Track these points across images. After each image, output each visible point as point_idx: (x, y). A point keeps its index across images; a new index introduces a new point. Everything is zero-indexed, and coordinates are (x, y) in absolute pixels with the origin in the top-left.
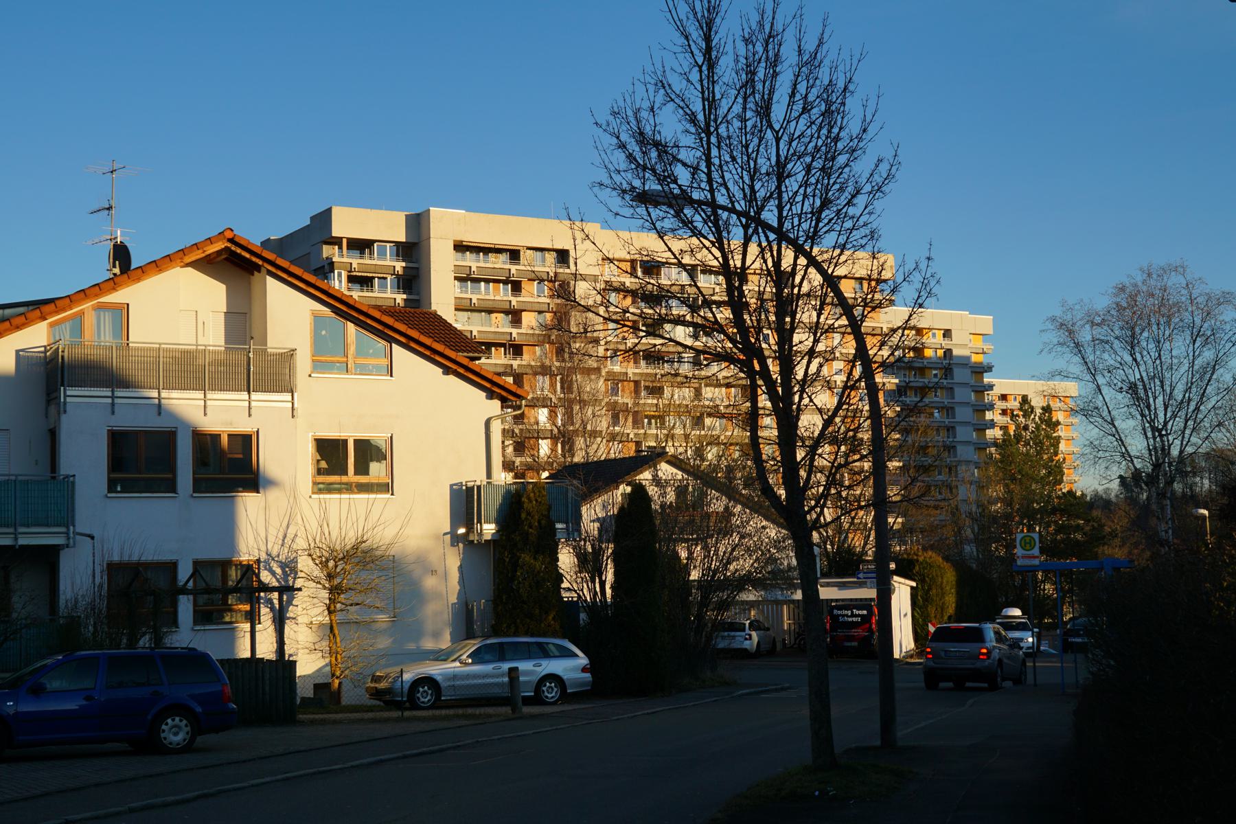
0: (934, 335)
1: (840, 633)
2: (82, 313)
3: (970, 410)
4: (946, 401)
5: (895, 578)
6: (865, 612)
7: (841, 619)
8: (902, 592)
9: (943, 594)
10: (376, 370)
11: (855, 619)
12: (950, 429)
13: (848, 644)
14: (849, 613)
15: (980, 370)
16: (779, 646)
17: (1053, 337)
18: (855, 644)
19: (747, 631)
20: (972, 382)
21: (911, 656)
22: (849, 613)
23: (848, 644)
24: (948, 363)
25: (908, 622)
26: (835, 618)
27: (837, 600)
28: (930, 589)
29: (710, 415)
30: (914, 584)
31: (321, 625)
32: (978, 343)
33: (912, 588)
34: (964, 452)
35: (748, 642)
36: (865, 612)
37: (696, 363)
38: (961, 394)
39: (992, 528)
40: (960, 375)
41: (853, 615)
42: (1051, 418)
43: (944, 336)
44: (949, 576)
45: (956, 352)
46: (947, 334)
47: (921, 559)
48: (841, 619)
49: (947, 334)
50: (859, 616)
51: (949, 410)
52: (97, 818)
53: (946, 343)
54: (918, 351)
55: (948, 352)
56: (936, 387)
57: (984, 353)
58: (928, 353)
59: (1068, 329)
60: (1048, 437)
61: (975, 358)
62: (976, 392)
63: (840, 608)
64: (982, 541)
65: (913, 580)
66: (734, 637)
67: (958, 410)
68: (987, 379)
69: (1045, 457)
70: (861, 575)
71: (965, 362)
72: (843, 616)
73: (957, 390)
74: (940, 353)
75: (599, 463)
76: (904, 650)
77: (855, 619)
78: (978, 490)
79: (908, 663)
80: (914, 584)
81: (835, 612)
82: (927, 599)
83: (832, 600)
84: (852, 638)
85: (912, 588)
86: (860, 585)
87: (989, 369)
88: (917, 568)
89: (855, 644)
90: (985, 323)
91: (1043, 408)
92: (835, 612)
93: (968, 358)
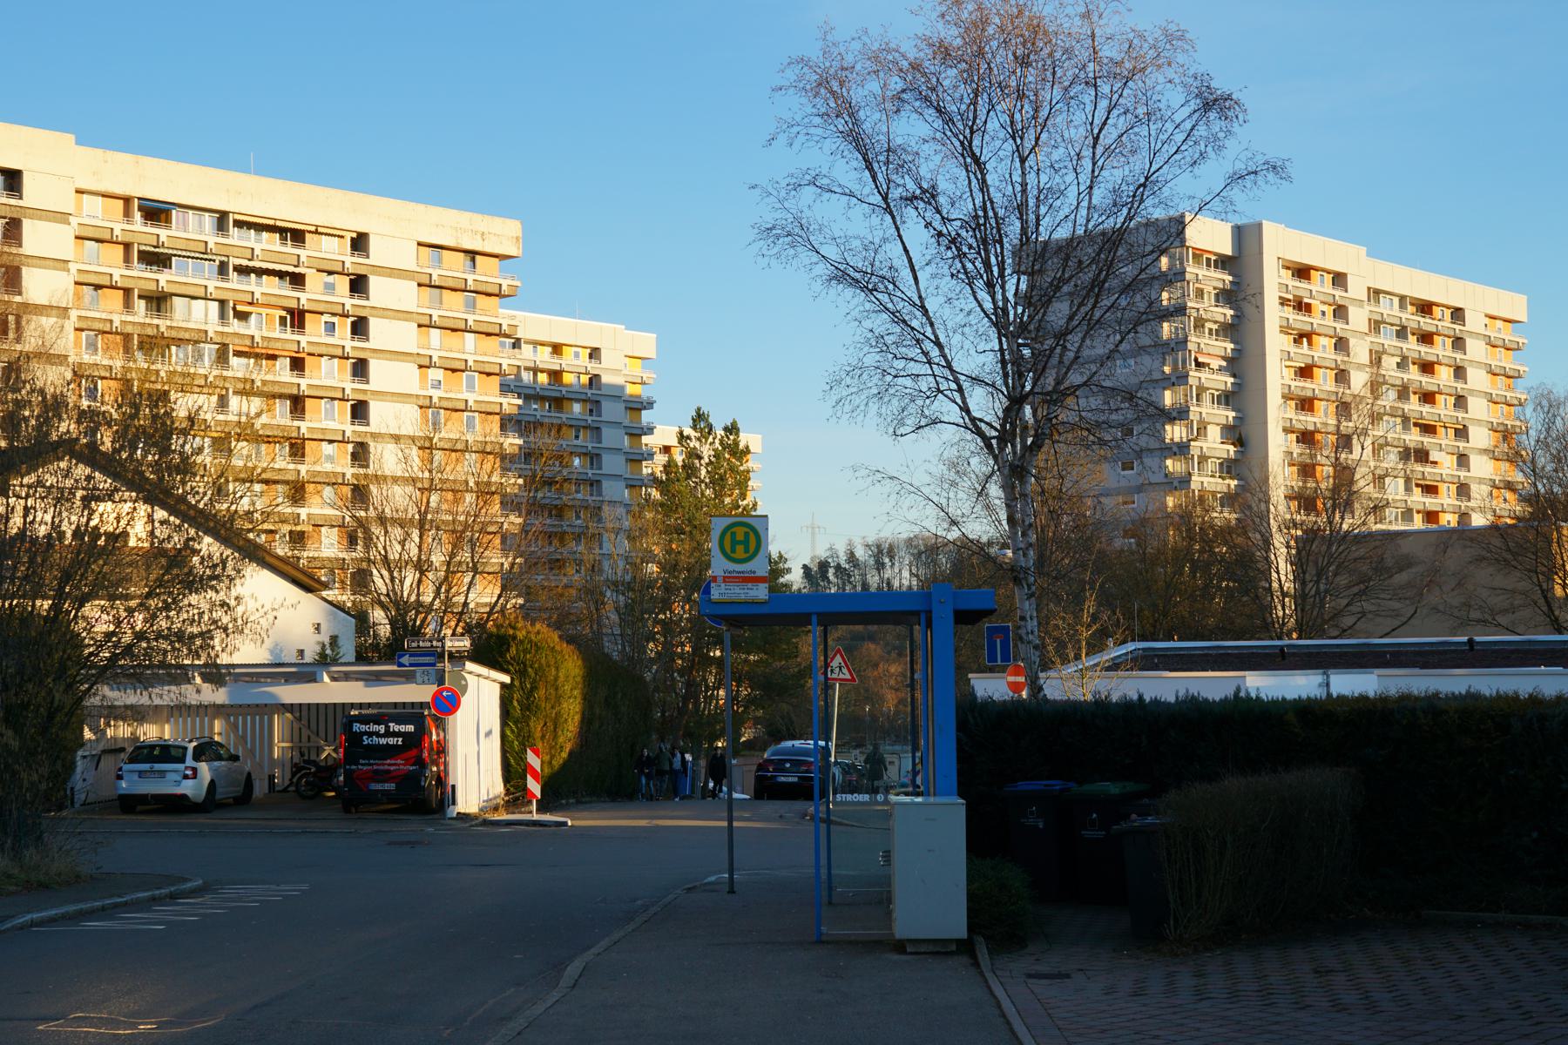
0: (577, 355)
1: (364, 766)
3: (623, 458)
4: (590, 446)
5: (469, 666)
6: (411, 728)
7: (366, 741)
8: (482, 692)
9: (558, 698)
11: (392, 741)
12: (594, 484)
13: (379, 787)
14: (382, 729)
15: (637, 406)
16: (260, 789)
17: (797, 106)
18: (391, 786)
19: (190, 762)
20: (626, 422)
21: (496, 809)
22: (382, 729)
23: (379, 787)
24: (594, 393)
25: (492, 751)
26: (354, 739)
27: (361, 706)
28: (534, 688)
29: (239, 437)
30: (507, 679)
32: (636, 369)
33: (503, 686)
34: (614, 490)
35: (190, 782)
36: (411, 728)
37: (222, 357)
38: (611, 437)
39: (641, 600)
40: (611, 411)
41: (388, 734)
42: (736, 443)
43: (591, 356)
44: (571, 667)
45: (605, 379)
46: (595, 353)
47: (521, 635)
48: (366, 741)
49: (595, 353)
51: (594, 458)
53: (593, 367)
54: (556, 375)
55: (594, 380)
56: (578, 427)
57: (643, 383)
58: (568, 378)
59: (831, 92)
60: (732, 469)
61: (631, 390)
62: (631, 435)
64: (631, 615)
65: (506, 671)
66: (162, 773)
67: (606, 458)
68: (646, 417)
69: (727, 500)
70: (405, 660)
71: (617, 394)
72: (370, 734)
73: (605, 431)
74: (585, 379)
77: (392, 741)
78: (629, 547)
79: (486, 823)
80: (507, 679)
81: (357, 727)
82: (528, 707)
83: (352, 706)
84: (385, 776)
85: (503, 686)
86: (409, 678)
87: (650, 405)
88: (513, 650)
89: (391, 786)
90: (646, 343)
91: (726, 429)
92: (357, 727)
93: (622, 388)
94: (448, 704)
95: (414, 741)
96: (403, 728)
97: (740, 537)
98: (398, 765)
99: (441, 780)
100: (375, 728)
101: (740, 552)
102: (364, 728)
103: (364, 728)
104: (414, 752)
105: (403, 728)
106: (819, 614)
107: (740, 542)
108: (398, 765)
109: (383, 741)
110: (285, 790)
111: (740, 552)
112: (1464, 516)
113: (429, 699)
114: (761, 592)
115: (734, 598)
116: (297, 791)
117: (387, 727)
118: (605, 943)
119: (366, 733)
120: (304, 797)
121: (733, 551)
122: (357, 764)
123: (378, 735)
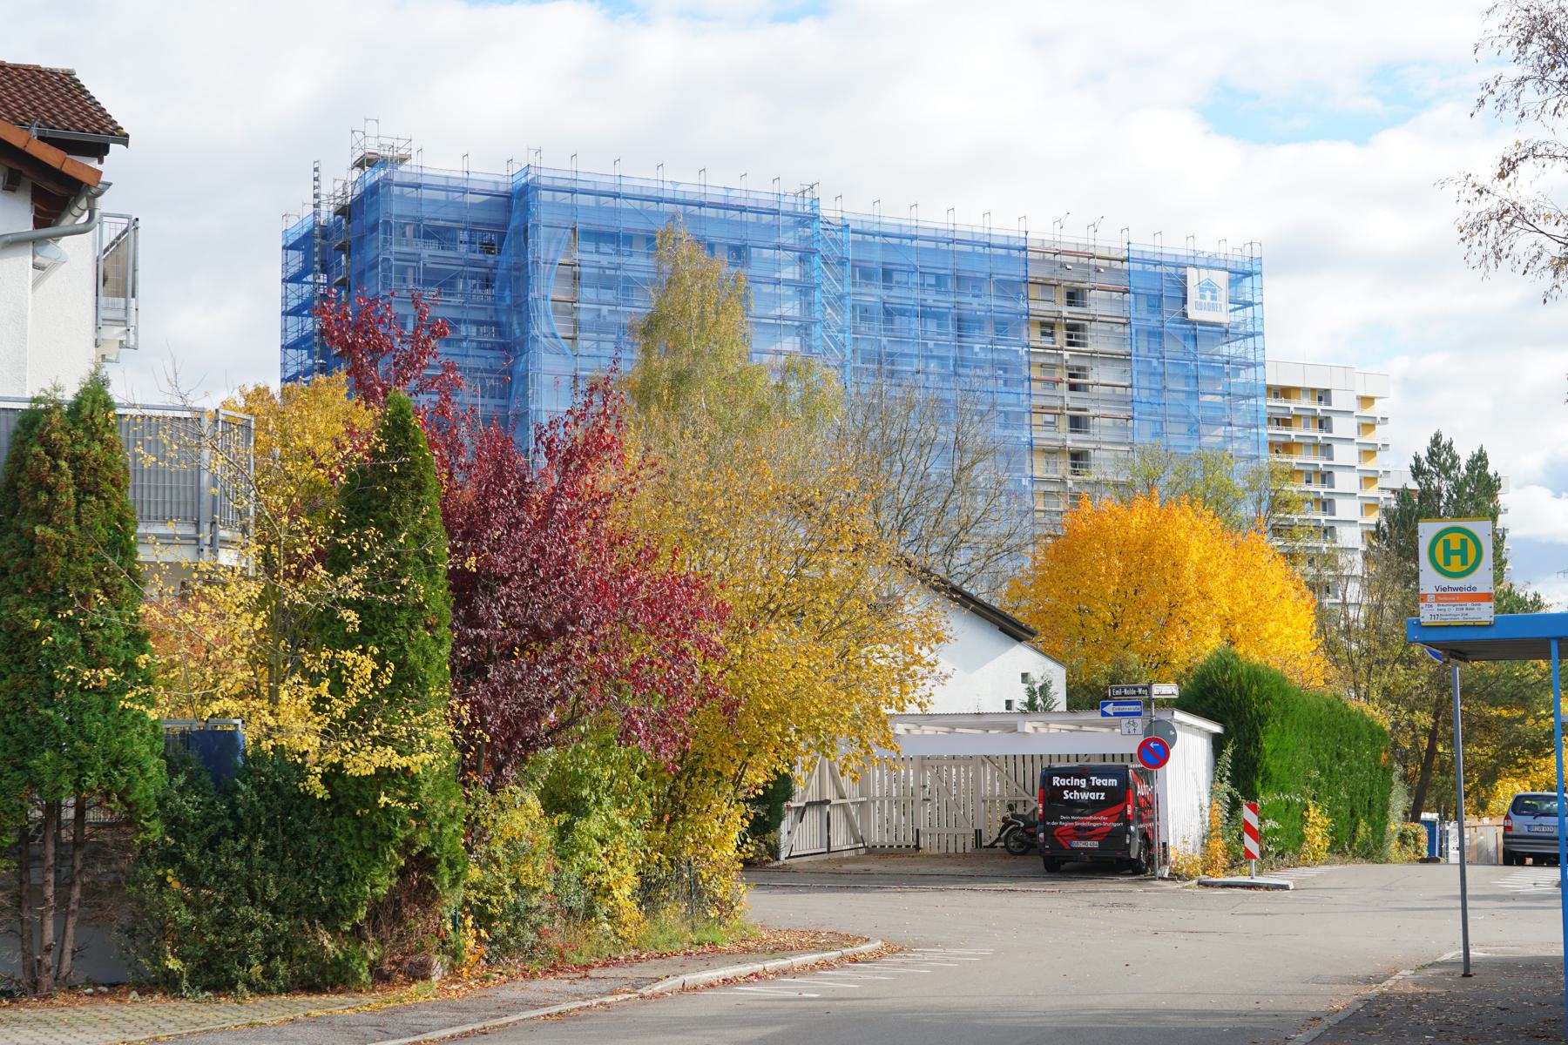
1: (1065, 822)
2: (1466, 717)
5: (1179, 716)
6: (1113, 782)
7: (1067, 795)
10: (285, 271)
11: (1093, 796)
13: (1081, 844)
14: (1083, 783)
23: (1081, 844)
30: (1217, 728)
31: (815, 202)
36: (1113, 782)
48: (1067, 795)
50: (1096, 789)
52: (466, 1035)
63: (1064, 773)
70: (1109, 709)
72: (1071, 789)
75: (63, 174)
76: (327, 189)
77: (1093, 796)
80: (1217, 728)
81: (1056, 781)
92: (1056, 781)
94: (1156, 753)
95: (1117, 797)
96: (1105, 782)
97: (1455, 545)
98: (1102, 821)
99: (1147, 840)
100: (1076, 782)
101: (1456, 564)
102: (1064, 782)
103: (1064, 782)
104: (1119, 808)
105: (1105, 782)
106: (1560, 639)
107: (1455, 553)
108: (1102, 821)
109: (1085, 796)
110: (992, 846)
111: (1456, 564)
112: (1386, 511)
113: (1135, 751)
114: (1484, 613)
115: (1450, 621)
116: (1006, 846)
117: (1089, 781)
118: (429, 1036)
119: (1066, 787)
120: (1012, 853)
121: (1448, 563)
122: (1058, 820)
123: (1079, 789)
